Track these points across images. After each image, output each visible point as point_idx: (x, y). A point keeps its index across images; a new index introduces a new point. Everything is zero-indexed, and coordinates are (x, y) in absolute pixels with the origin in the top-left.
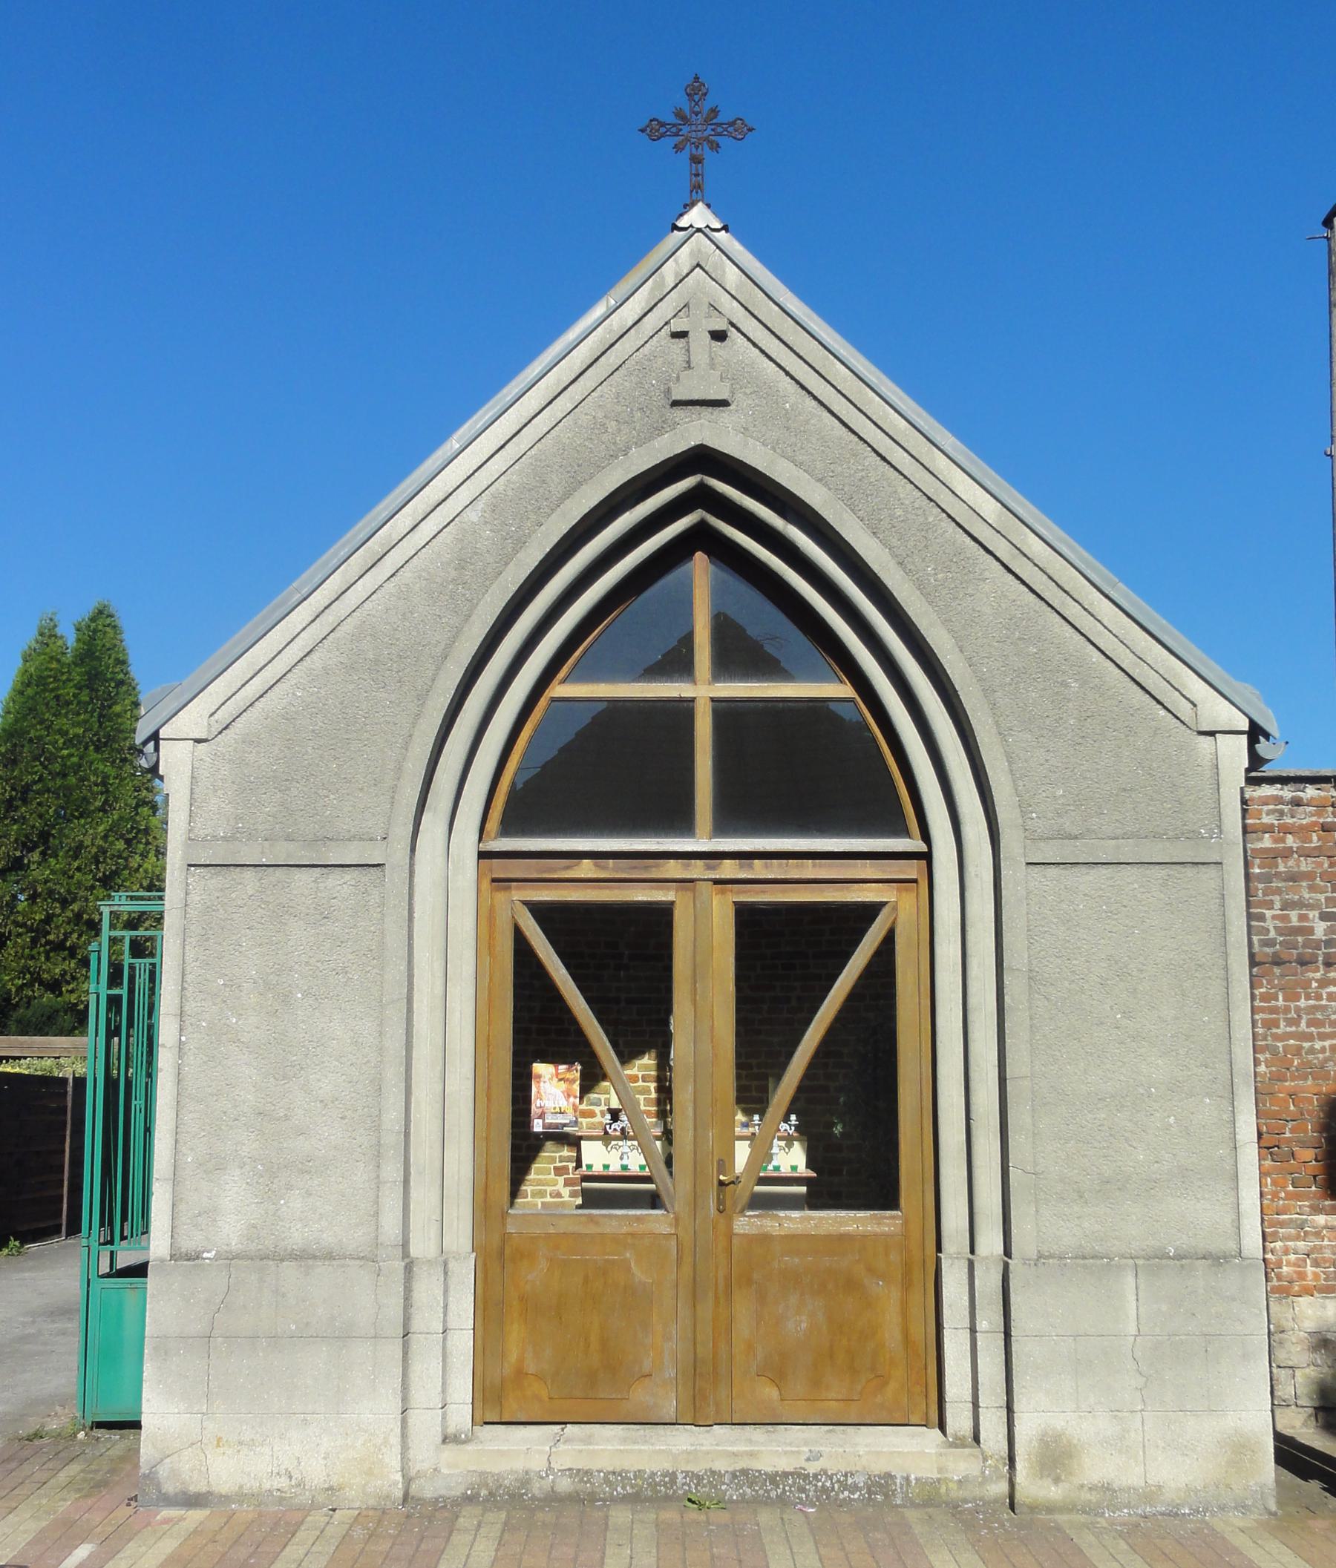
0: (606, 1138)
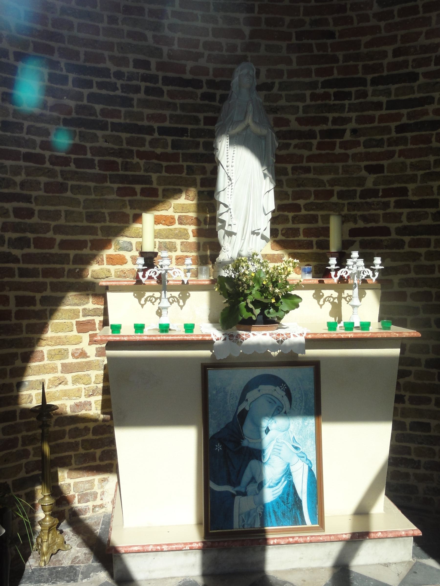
0: (138, 287)
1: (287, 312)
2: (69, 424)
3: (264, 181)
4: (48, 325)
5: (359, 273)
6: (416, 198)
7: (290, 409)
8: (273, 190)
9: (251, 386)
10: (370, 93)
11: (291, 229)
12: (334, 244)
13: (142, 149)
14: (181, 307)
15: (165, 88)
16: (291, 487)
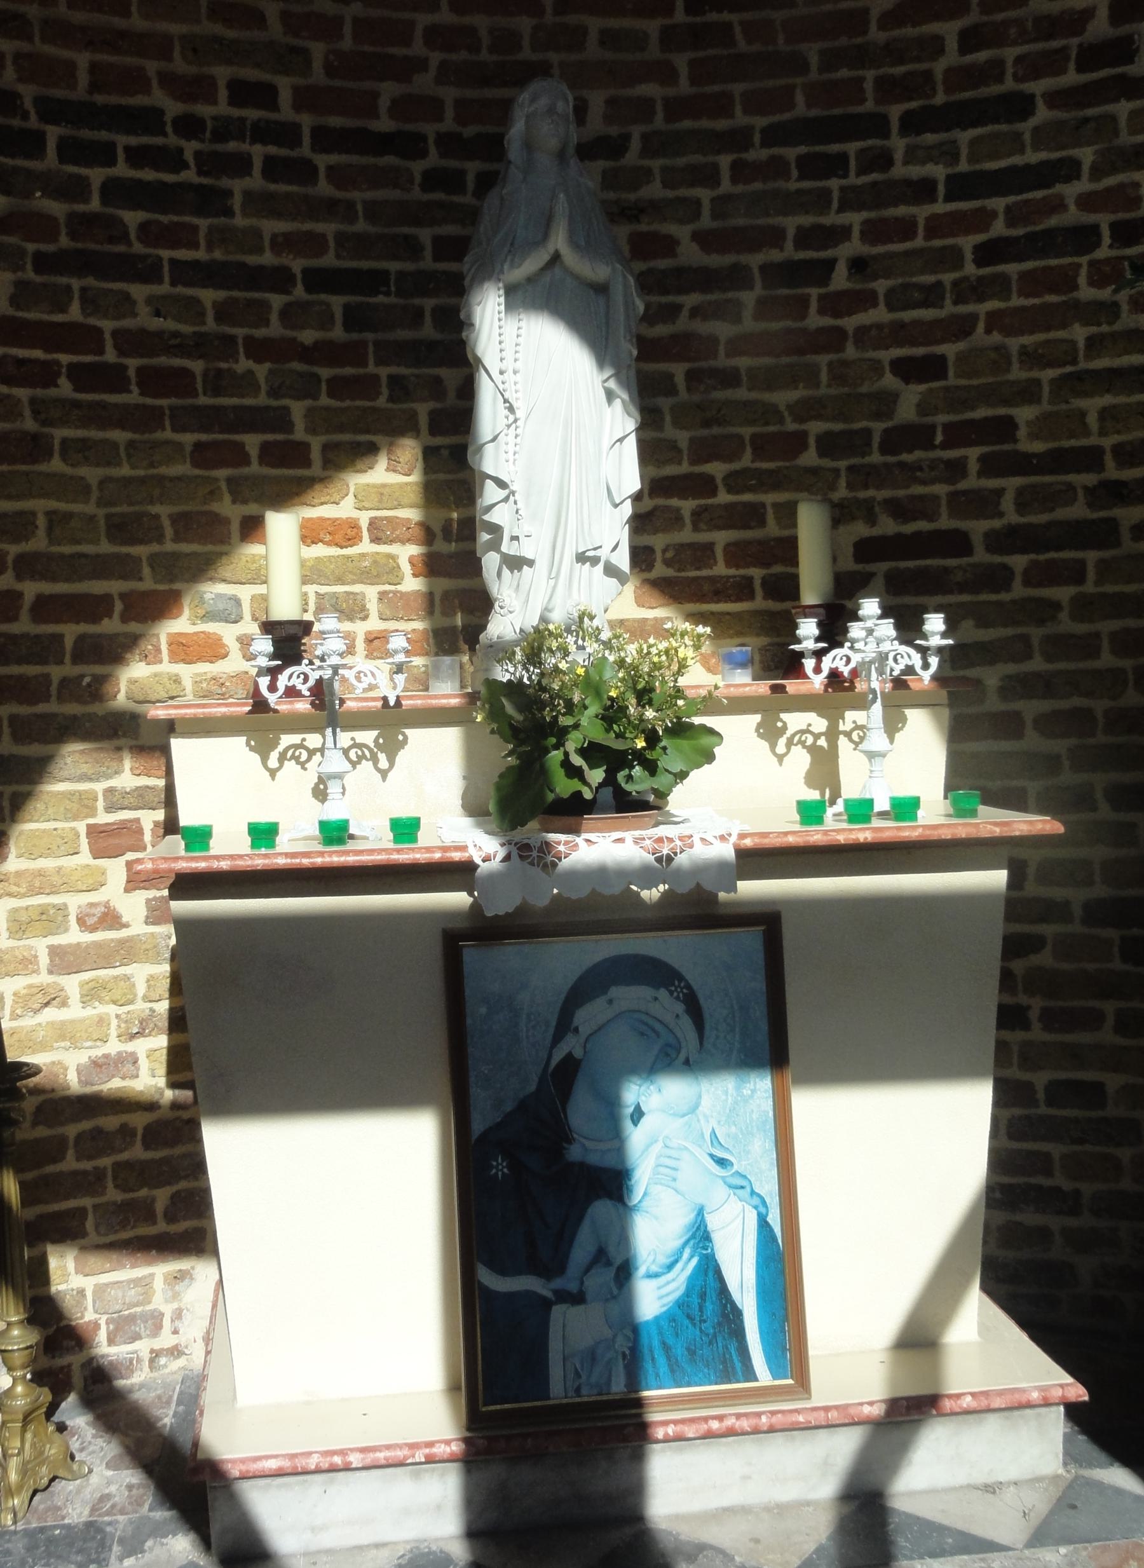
0: (259, 722)
1: (682, 776)
2: (76, 1118)
3: (608, 411)
4: (8, 839)
5: (883, 657)
6: (1038, 447)
7: (700, 1052)
8: (633, 436)
9: (583, 990)
10: (899, 156)
11: (691, 546)
12: (813, 589)
13: (260, 333)
14: (384, 774)
15: (322, 161)
16: (711, 1274)
